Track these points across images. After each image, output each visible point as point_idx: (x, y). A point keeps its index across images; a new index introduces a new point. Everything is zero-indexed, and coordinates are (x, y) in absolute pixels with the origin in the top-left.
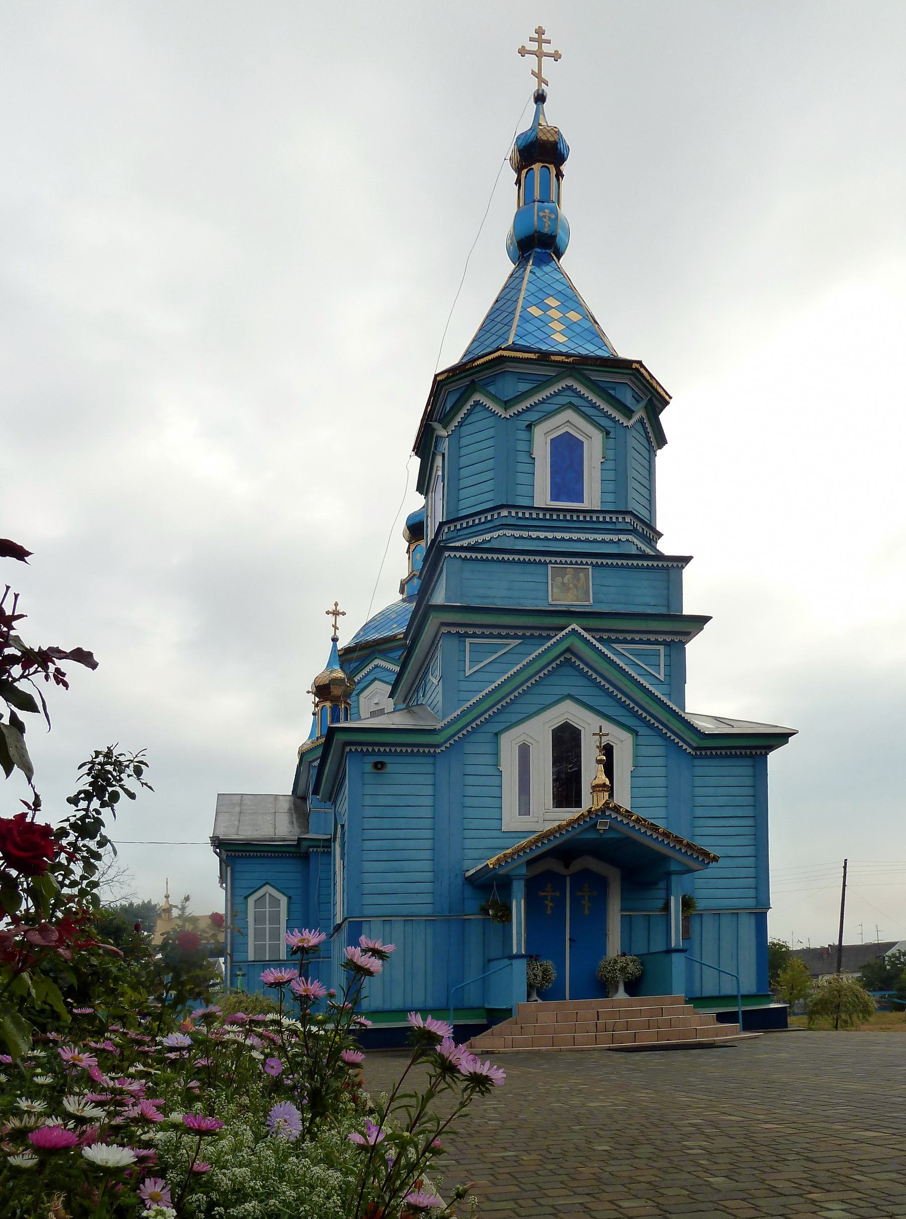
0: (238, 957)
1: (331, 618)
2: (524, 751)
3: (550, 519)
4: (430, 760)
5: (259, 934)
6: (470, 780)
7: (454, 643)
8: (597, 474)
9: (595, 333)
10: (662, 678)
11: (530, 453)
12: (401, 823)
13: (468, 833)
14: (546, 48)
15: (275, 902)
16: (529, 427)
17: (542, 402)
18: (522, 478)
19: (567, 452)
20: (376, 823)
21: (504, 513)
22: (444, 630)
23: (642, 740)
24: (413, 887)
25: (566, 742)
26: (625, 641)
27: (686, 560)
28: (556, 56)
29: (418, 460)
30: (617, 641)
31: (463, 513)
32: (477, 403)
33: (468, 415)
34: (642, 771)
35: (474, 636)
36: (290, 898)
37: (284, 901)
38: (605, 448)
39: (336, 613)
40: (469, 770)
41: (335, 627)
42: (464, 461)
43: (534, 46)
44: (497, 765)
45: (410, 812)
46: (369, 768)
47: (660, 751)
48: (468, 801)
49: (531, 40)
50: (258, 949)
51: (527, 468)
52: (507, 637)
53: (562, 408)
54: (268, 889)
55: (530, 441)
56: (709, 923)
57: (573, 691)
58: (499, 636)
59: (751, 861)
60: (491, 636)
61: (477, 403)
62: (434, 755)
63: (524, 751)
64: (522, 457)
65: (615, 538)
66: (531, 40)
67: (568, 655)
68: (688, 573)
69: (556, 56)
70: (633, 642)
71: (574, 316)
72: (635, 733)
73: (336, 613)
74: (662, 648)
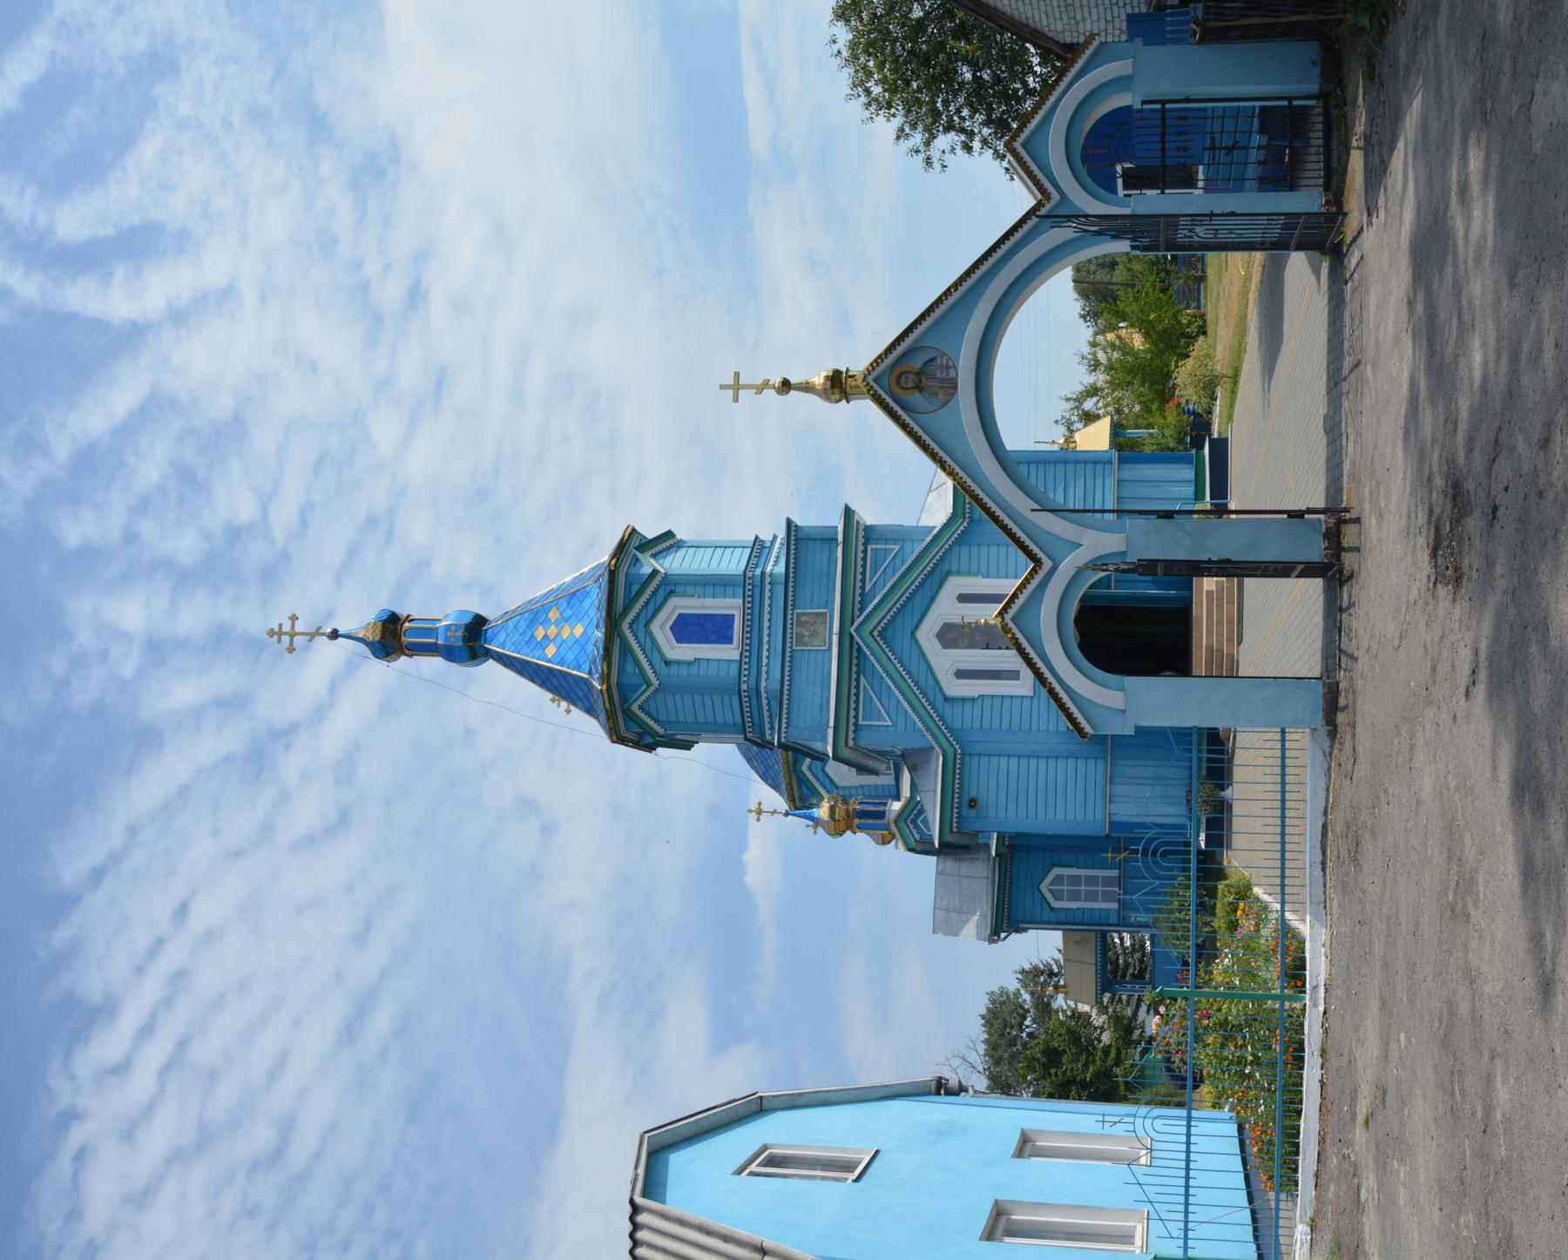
0: (1113, 919)
1: (764, 817)
2: (961, 674)
3: (751, 648)
4: (967, 758)
5: (1091, 897)
6: (986, 724)
7: (863, 734)
8: (709, 602)
9: (571, 596)
10: (897, 547)
11: (689, 664)
12: (1022, 784)
13: (1034, 727)
14: (287, 628)
15: (1058, 880)
16: (667, 663)
17: (643, 650)
18: (712, 671)
19: (688, 629)
20: (1022, 807)
21: (744, 687)
22: (851, 743)
23: (954, 568)
24: (1081, 778)
25: (952, 636)
26: (863, 581)
27: (789, 522)
28: (294, 618)
29: (659, 750)
30: (863, 587)
31: (739, 721)
32: (640, 707)
33: (653, 718)
34: (983, 568)
35: (856, 717)
36: (1055, 865)
37: (1057, 871)
38: (685, 595)
39: (759, 812)
40: (977, 724)
41: (774, 812)
42: (691, 719)
43: (286, 639)
44: (973, 700)
45: (1013, 777)
46: (972, 812)
47: (965, 550)
48: (1005, 726)
49: (279, 641)
50: (1107, 897)
51: (703, 665)
52: (857, 687)
53: (648, 632)
54: (1044, 887)
55: (679, 663)
56: (1126, 492)
57: (908, 629)
58: (857, 695)
59: (1070, 468)
60: (857, 702)
61: (640, 707)
62: (963, 754)
63: (961, 674)
64: (693, 670)
65: (768, 587)
66: (279, 641)
67: (876, 633)
68: (799, 521)
69: (294, 618)
70: (863, 573)
71: (553, 615)
72: (949, 573)
73: (759, 812)
74: (870, 547)
